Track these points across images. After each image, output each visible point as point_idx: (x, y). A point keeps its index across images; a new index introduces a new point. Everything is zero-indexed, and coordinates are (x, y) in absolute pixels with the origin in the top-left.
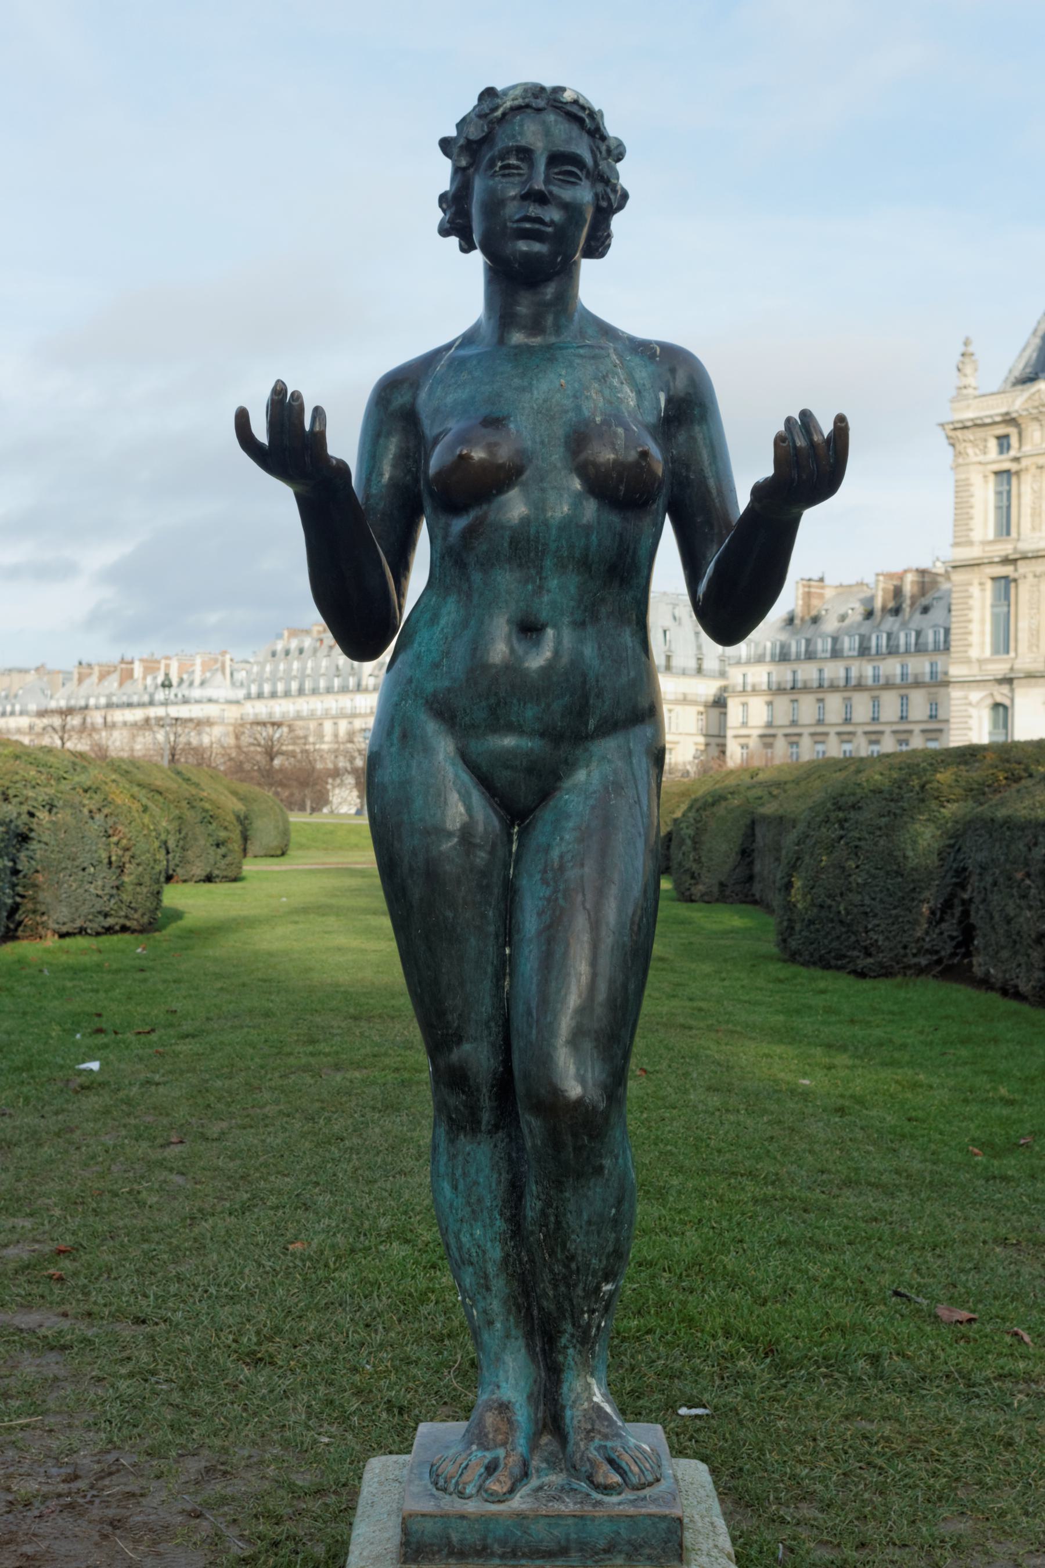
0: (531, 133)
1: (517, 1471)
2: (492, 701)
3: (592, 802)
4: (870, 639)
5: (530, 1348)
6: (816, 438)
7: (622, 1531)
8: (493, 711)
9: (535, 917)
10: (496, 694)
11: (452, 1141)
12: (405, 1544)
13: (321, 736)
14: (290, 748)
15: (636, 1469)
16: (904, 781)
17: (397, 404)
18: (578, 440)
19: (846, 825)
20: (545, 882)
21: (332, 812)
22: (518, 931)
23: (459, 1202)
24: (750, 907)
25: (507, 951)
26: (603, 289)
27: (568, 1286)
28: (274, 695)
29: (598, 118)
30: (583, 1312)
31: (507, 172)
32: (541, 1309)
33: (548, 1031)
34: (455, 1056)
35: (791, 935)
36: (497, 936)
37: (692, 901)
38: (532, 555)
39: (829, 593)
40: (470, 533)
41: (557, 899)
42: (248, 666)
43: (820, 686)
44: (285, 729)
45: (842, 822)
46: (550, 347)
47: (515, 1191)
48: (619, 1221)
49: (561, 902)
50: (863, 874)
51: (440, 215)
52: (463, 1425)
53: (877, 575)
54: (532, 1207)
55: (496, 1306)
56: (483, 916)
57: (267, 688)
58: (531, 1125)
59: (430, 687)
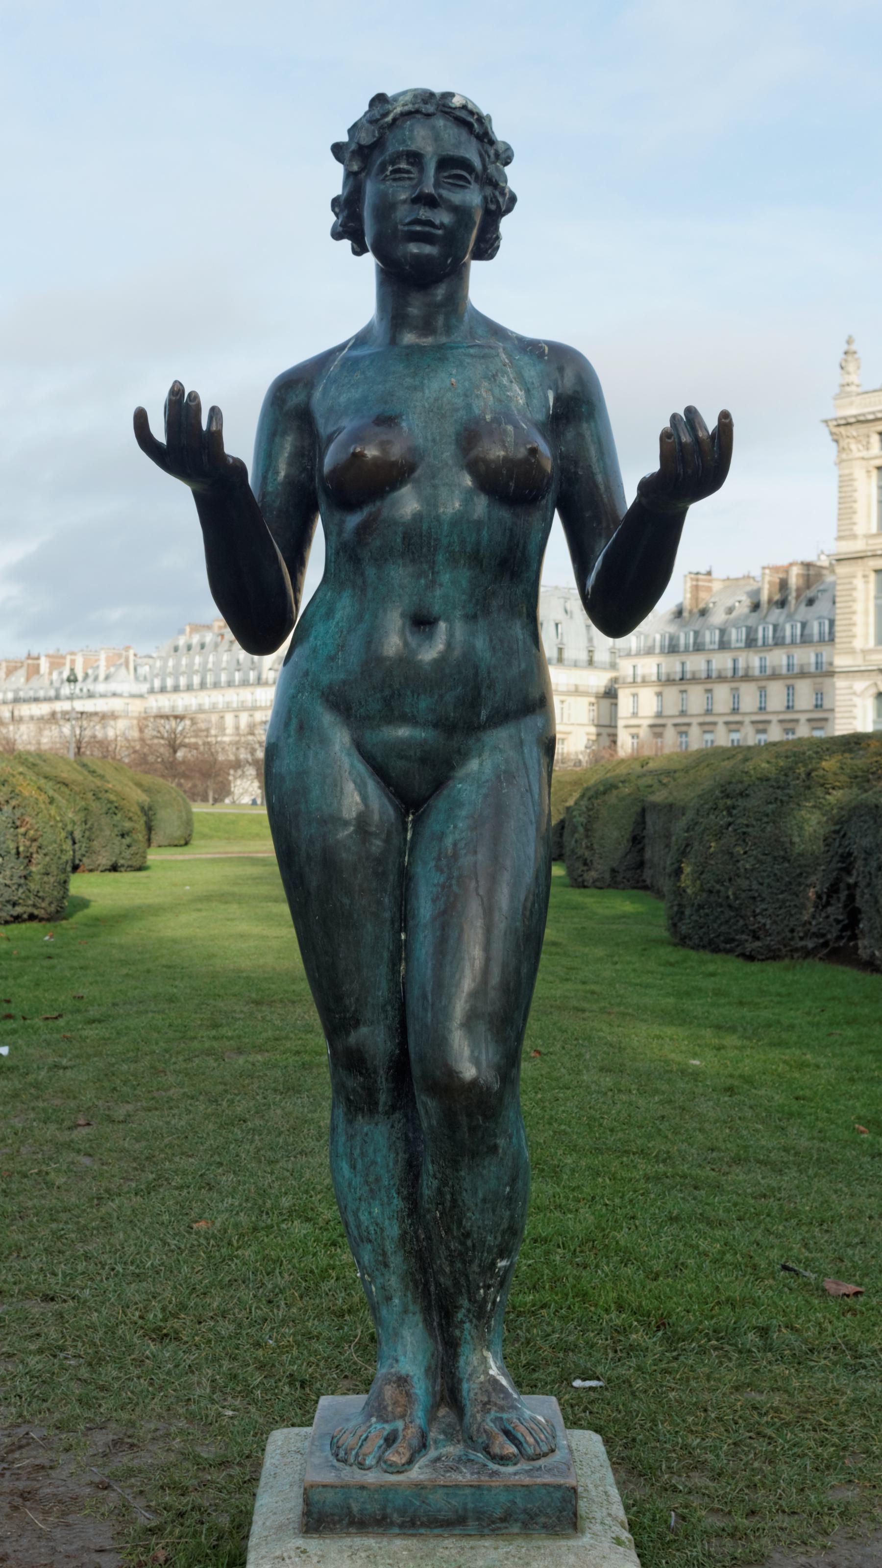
0: (420, 138)
1: (415, 1442)
2: (387, 692)
3: (484, 791)
4: (756, 631)
5: (428, 1322)
6: (700, 434)
7: (518, 1500)
8: (387, 702)
9: (429, 903)
10: (390, 686)
11: (350, 1122)
12: (307, 1514)
13: (222, 729)
14: (193, 740)
15: (531, 1440)
16: (791, 768)
17: (292, 402)
18: (469, 437)
19: (734, 812)
20: (439, 869)
21: (234, 802)
22: (413, 917)
23: (358, 1181)
24: (641, 893)
25: (403, 937)
26: (493, 290)
27: (464, 1262)
28: (176, 689)
29: (486, 122)
30: (479, 1288)
31: (398, 176)
32: (438, 1284)
33: (443, 1013)
34: (353, 1039)
35: (681, 919)
36: (393, 922)
37: (585, 887)
38: (424, 550)
39: (716, 586)
40: (364, 530)
41: (451, 886)
42: (151, 661)
43: (709, 677)
44: (188, 722)
45: (730, 809)
46: (440, 347)
47: (412, 1170)
48: (513, 1199)
49: (455, 888)
50: (750, 859)
51: (333, 218)
52: (363, 1398)
53: (764, 568)
54: (428, 1186)
55: (394, 1282)
56: (379, 903)
57: (170, 682)
58: (428, 1107)
59: (325, 679)
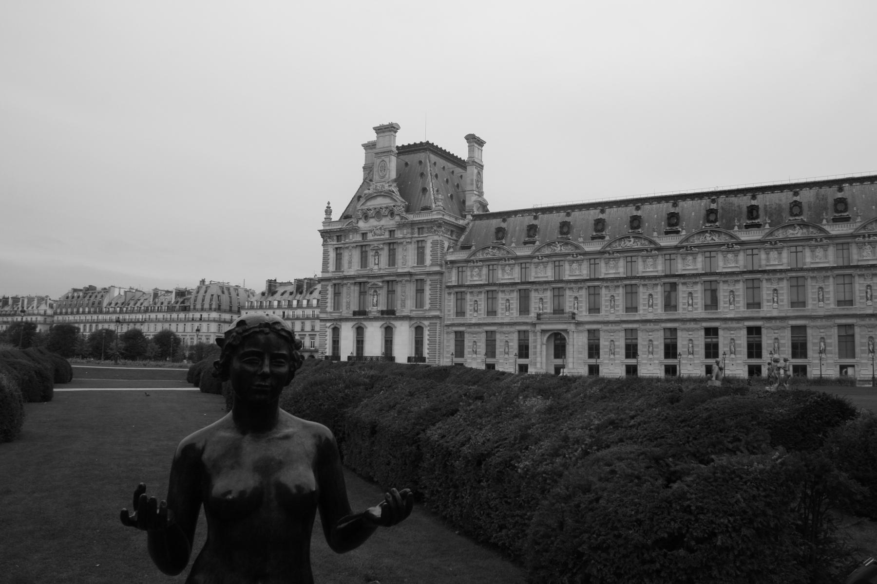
28: (66, 313)
